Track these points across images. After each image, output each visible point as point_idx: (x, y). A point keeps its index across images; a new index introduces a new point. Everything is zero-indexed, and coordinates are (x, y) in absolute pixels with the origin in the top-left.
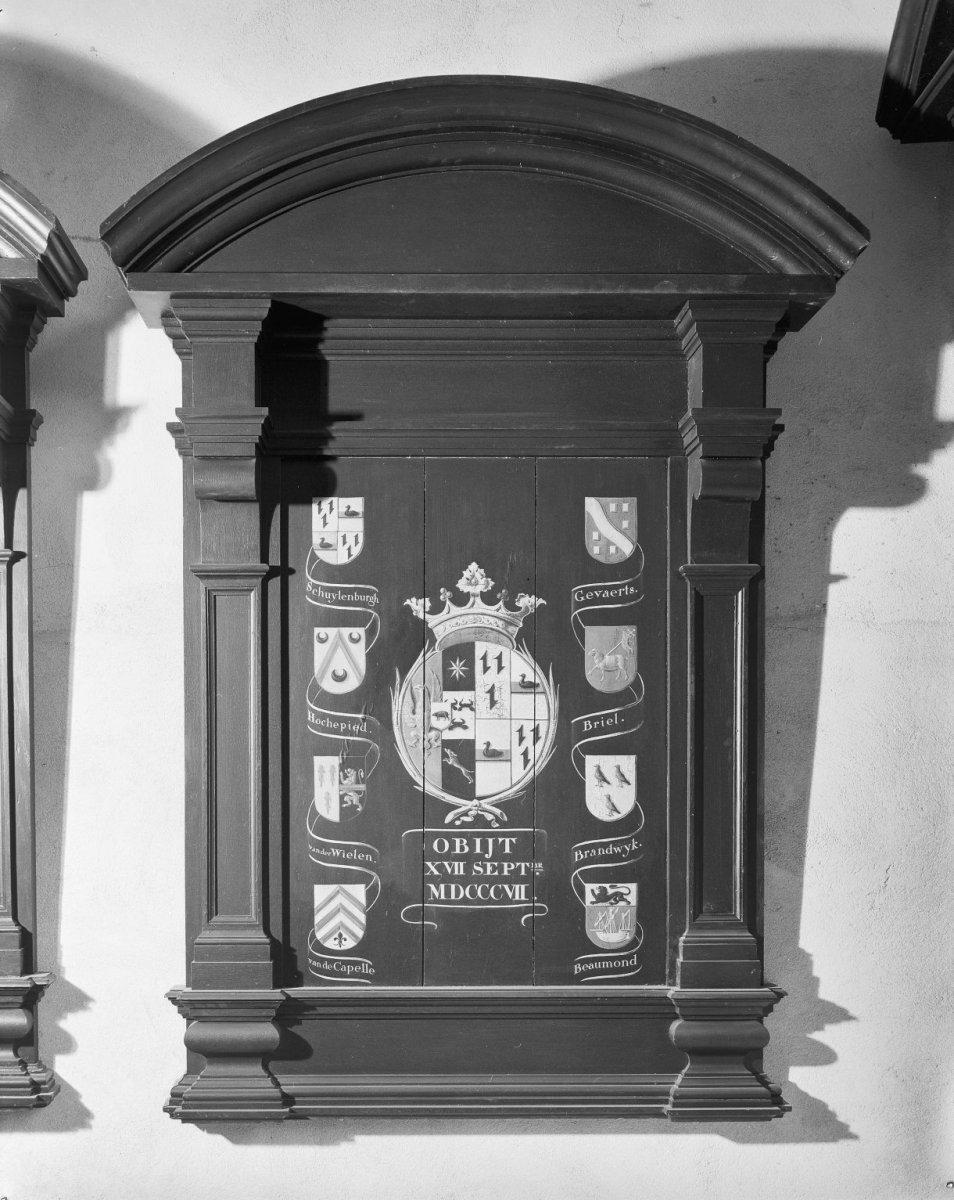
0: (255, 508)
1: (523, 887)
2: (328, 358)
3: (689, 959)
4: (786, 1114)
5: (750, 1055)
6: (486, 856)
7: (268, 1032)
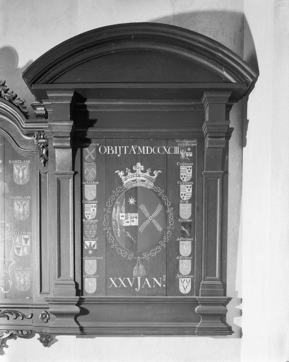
0: (71, 150)
1: (175, 153)
2: (89, 110)
3: (204, 296)
4: (233, 334)
5: (222, 317)
6: (118, 156)
7: (77, 309)
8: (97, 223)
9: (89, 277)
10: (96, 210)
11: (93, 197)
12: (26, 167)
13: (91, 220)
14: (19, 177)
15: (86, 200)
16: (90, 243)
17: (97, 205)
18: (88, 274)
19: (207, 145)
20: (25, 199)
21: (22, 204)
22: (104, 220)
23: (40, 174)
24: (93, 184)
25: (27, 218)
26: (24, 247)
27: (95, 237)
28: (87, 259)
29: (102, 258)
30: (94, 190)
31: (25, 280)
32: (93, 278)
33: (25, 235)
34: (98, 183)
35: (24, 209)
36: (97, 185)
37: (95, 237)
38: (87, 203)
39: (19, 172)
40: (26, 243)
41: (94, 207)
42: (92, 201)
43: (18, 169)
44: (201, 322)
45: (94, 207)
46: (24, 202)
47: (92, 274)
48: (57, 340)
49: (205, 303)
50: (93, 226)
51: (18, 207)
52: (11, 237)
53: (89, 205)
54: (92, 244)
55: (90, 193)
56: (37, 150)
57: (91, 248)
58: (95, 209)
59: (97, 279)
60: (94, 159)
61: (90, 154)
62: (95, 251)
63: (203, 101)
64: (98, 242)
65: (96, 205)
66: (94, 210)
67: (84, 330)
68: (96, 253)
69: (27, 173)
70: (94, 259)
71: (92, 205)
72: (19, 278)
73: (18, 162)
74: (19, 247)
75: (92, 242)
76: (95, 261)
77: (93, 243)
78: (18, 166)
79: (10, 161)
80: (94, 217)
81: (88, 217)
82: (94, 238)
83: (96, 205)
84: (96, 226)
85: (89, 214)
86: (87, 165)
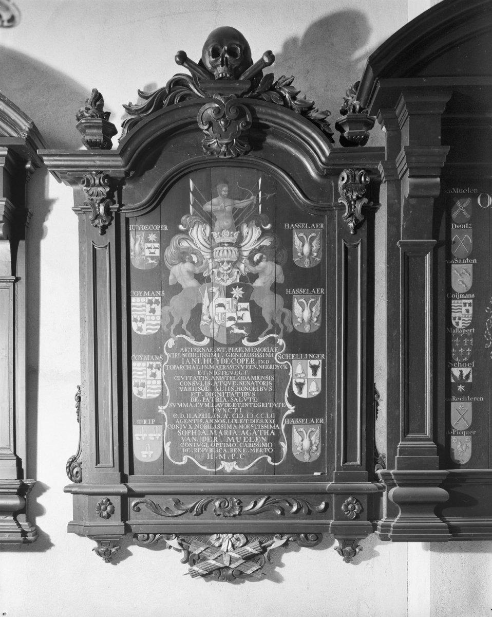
7: (15, 501)
8: (474, 335)
9: (459, 435)
10: (471, 312)
11: (466, 286)
12: (317, 235)
13: (462, 329)
14: (302, 254)
15: (455, 293)
16: (461, 371)
17: (473, 301)
18: (457, 428)
19: (406, 190)
20: (313, 294)
21: (307, 304)
22: (486, 329)
23: (94, 250)
24: (467, 263)
25: (317, 329)
26: (310, 380)
27: (470, 361)
28: (454, 401)
29: (482, 399)
30: (468, 275)
31: (311, 441)
32: (466, 435)
33: (313, 359)
34: (475, 261)
35: (312, 312)
36: (474, 265)
37: (470, 361)
38: (456, 299)
39: (303, 246)
40: (315, 374)
41: (467, 305)
42: (465, 294)
43: (301, 239)
44: (399, 516)
45: (467, 305)
46: (313, 300)
47: (464, 429)
48: (130, 554)
49: (405, 481)
50: (466, 340)
51: (301, 309)
52: (287, 363)
53: (459, 301)
54: (465, 374)
55: (461, 281)
56: (89, 207)
57: (461, 380)
58: (471, 309)
59: (472, 437)
60: (468, 216)
61: (461, 208)
62: (469, 387)
63: (397, 112)
64: (474, 370)
65: (471, 301)
66: (467, 311)
67: (27, 536)
68: (471, 390)
69: (318, 247)
70: (467, 401)
71: (464, 301)
72: (300, 438)
73: (301, 226)
74: (302, 381)
75: (463, 369)
76: (469, 405)
77: (466, 371)
78: (301, 235)
79: (287, 225)
80: (467, 324)
81: (457, 324)
82: (467, 362)
83: (471, 301)
84: (472, 340)
85: (459, 318)
86: (457, 228)
